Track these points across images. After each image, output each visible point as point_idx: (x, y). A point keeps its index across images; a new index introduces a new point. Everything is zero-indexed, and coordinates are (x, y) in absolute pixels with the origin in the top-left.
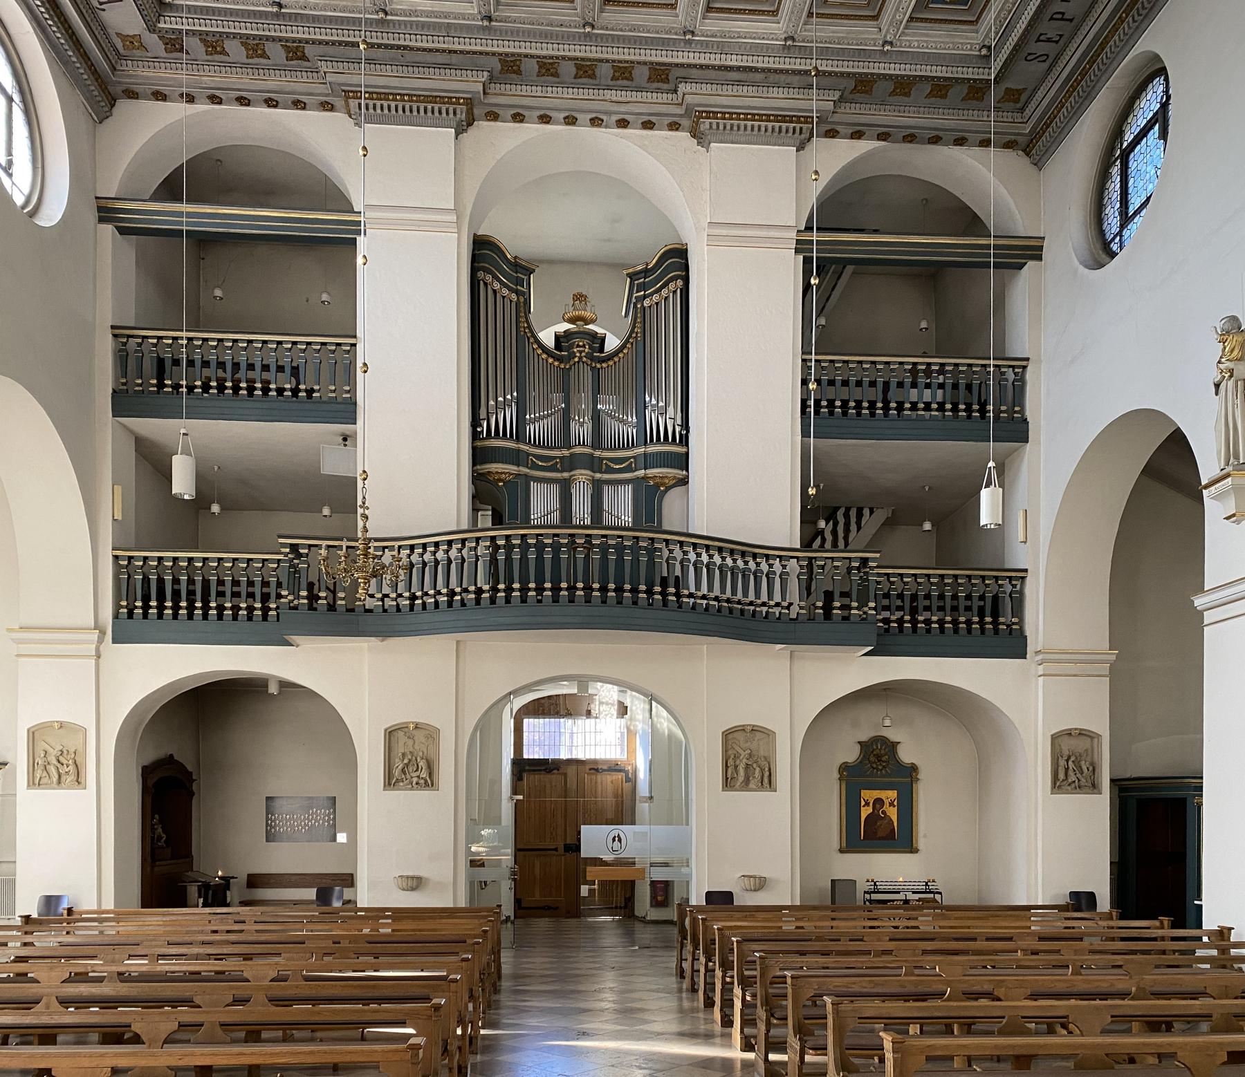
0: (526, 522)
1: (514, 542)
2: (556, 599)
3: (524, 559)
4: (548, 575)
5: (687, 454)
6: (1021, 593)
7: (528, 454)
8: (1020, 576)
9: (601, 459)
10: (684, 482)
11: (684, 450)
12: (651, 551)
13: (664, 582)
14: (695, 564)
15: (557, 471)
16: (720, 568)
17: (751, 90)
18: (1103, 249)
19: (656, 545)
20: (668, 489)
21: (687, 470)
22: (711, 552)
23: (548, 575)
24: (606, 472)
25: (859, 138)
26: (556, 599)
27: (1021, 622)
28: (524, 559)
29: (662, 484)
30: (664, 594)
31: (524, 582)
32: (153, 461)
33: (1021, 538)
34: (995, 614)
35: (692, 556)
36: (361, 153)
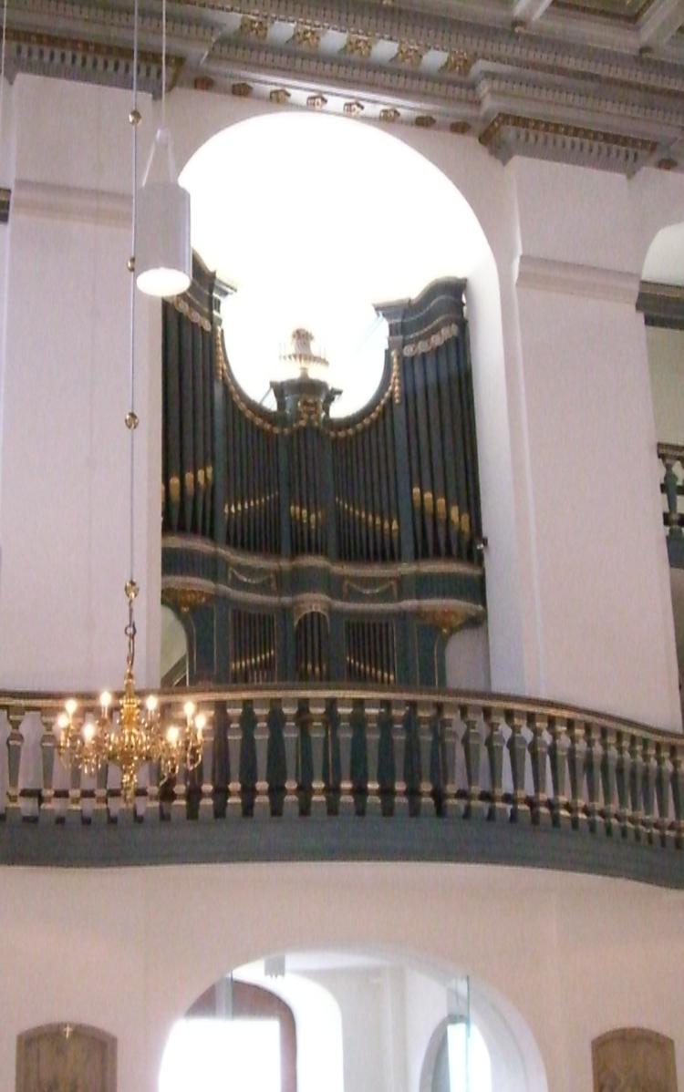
1: (421, 714)
2: (388, 810)
3: (276, 744)
5: (482, 579)
10: (477, 622)
11: (477, 572)
12: (438, 725)
14: (465, 741)
16: (533, 747)
19: (447, 716)
20: (453, 631)
21: (484, 603)
22: (471, 717)
23: (373, 769)
26: (388, 810)
28: (276, 744)
29: (445, 625)
31: (386, 779)
32: (92, 44)
34: (440, 772)
35: (505, 731)
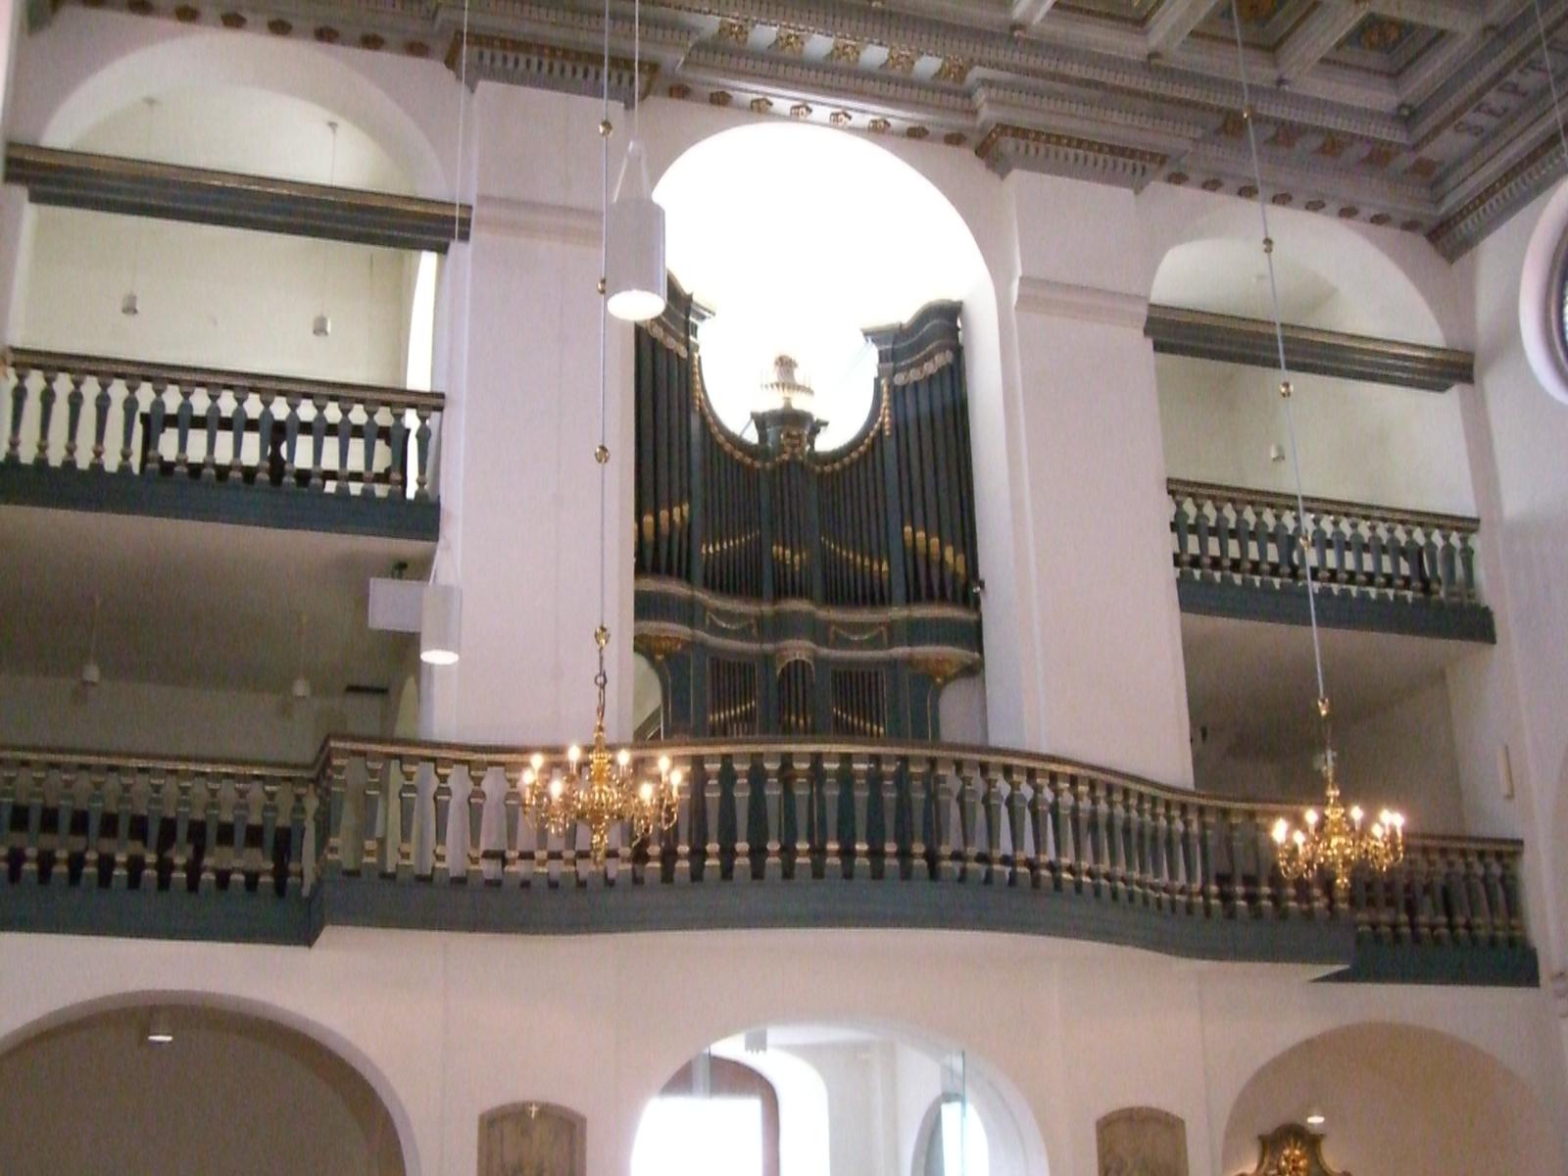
0: (936, 742)
4: (861, 828)
5: (979, 625)
6: (1514, 877)
7: (705, 608)
8: (1508, 852)
9: (828, 624)
10: (973, 670)
11: (973, 617)
12: (932, 782)
13: (1250, 881)
14: (961, 799)
15: (749, 638)
17: (1081, 110)
18: (809, 391)
20: (947, 680)
21: (981, 651)
23: (861, 828)
24: (834, 647)
25: (1214, 190)
26: (878, 873)
27: (1522, 928)
30: (1252, 898)
33: (1505, 790)
35: (1004, 788)
36: (601, 129)
